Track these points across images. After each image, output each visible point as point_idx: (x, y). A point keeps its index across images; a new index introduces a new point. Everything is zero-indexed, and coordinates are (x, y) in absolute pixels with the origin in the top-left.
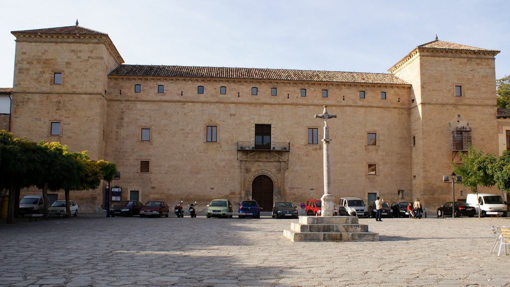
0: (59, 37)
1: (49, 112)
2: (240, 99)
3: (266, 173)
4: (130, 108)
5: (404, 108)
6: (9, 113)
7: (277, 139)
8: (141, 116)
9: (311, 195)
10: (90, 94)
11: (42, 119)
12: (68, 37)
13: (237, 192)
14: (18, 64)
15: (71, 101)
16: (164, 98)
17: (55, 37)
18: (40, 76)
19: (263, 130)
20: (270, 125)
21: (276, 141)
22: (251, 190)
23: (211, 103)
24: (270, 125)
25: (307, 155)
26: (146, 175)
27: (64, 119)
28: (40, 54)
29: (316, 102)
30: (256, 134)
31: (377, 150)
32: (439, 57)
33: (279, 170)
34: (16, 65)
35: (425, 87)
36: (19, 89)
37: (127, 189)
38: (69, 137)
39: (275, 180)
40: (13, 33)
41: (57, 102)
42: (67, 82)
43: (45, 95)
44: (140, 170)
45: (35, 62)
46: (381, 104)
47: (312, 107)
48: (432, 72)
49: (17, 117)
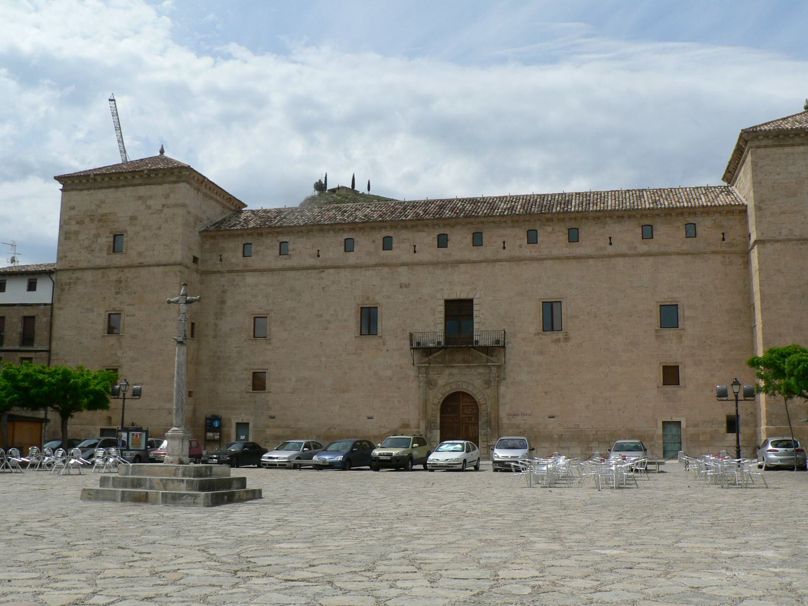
0: (121, 178)
1: (105, 298)
2: (418, 257)
3: (464, 388)
4: (236, 283)
5: (735, 253)
6: (49, 302)
7: (484, 325)
8: (253, 296)
9: (551, 427)
10: (164, 265)
11: (96, 309)
12: (134, 177)
13: (413, 423)
14: (64, 226)
15: (136, 277)
16: (288, 263)
17: (116, 178)
18: (93, 242)
19: (459, 312)
20: (471, 301)
21: (482, 328)
22: (439, 419)
23: (367, 267)
24: (471, 301)
25: (541, 353)
26: (260, 396)
27: (126, 307)
28: (94, 207)
29: (555, 252)
30: (447, 317)
31: (681, 337)
32: (793, 145)
33: (488, 383)
34: (61, 227)
35: (763, 207)
36: (65, 264)
37: (230, 420)
38: (134, 337)
39: (482, 401)
40: (59, 178)
41: (116, 281)
42: (131, 248)
43: (100, 271)
44: (251, 388)
45: (87, 220)
46: (685, 248)
47: (549, 261)
48: (777, 177)
49: (61, 309)
